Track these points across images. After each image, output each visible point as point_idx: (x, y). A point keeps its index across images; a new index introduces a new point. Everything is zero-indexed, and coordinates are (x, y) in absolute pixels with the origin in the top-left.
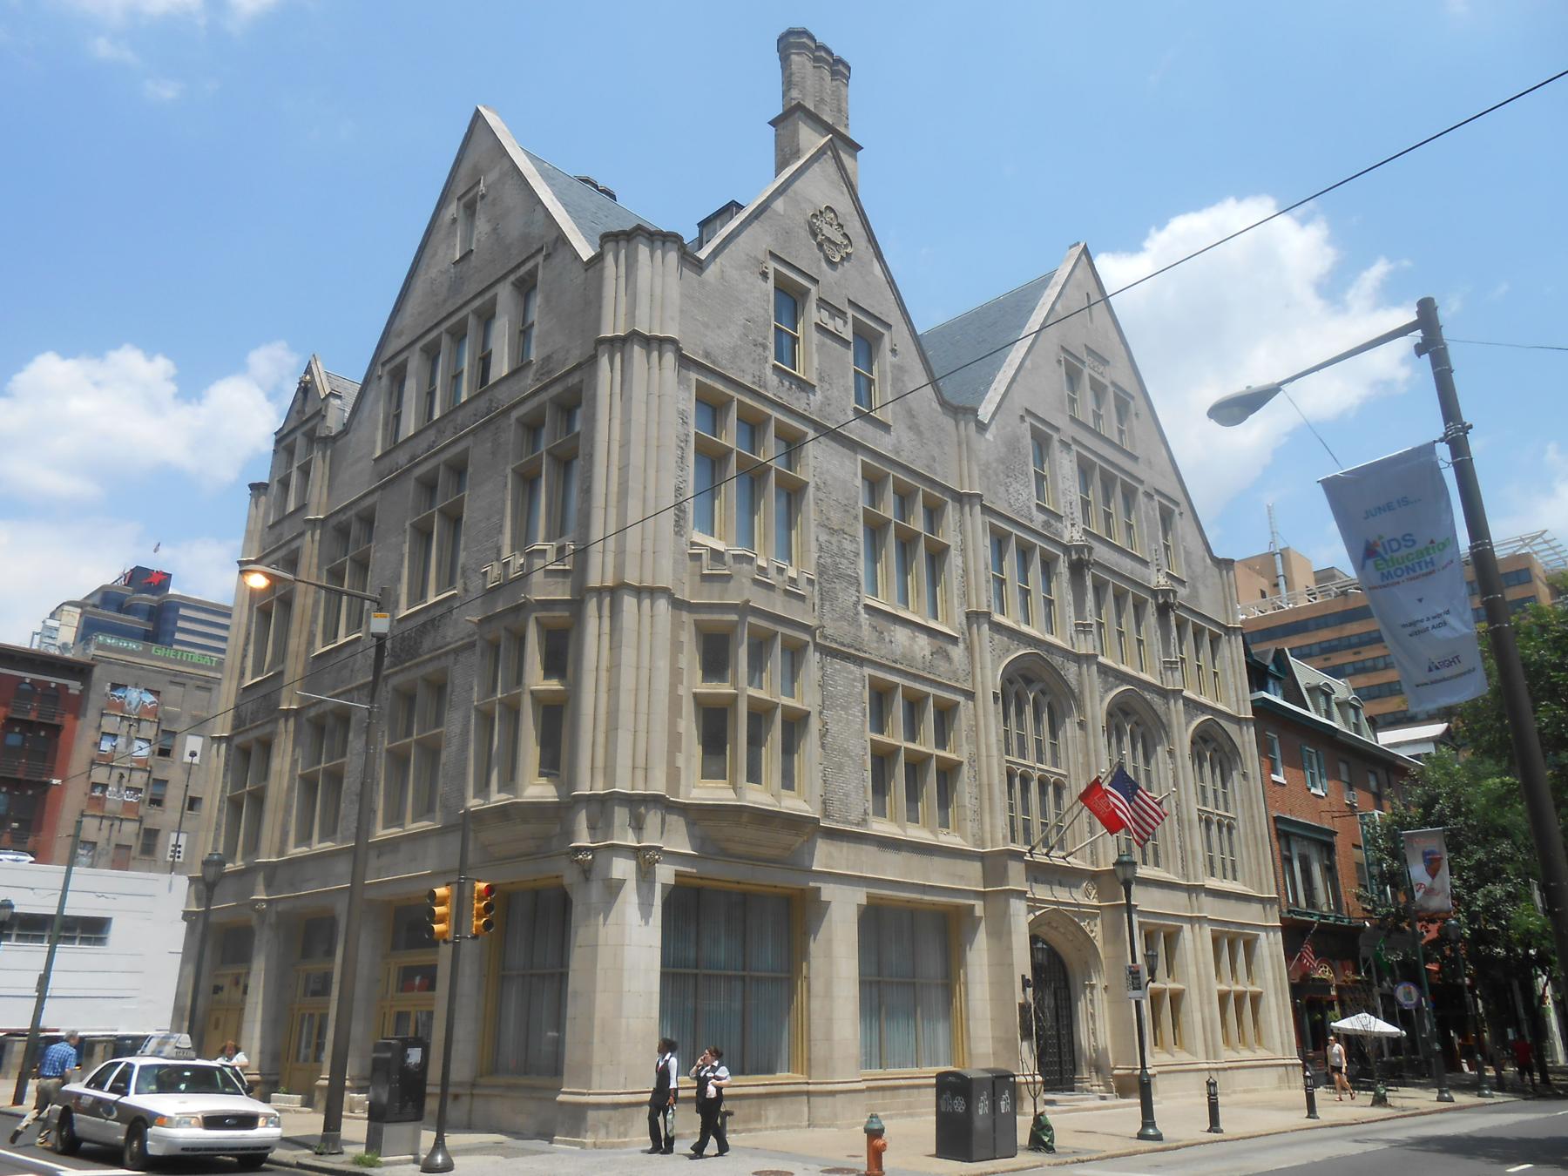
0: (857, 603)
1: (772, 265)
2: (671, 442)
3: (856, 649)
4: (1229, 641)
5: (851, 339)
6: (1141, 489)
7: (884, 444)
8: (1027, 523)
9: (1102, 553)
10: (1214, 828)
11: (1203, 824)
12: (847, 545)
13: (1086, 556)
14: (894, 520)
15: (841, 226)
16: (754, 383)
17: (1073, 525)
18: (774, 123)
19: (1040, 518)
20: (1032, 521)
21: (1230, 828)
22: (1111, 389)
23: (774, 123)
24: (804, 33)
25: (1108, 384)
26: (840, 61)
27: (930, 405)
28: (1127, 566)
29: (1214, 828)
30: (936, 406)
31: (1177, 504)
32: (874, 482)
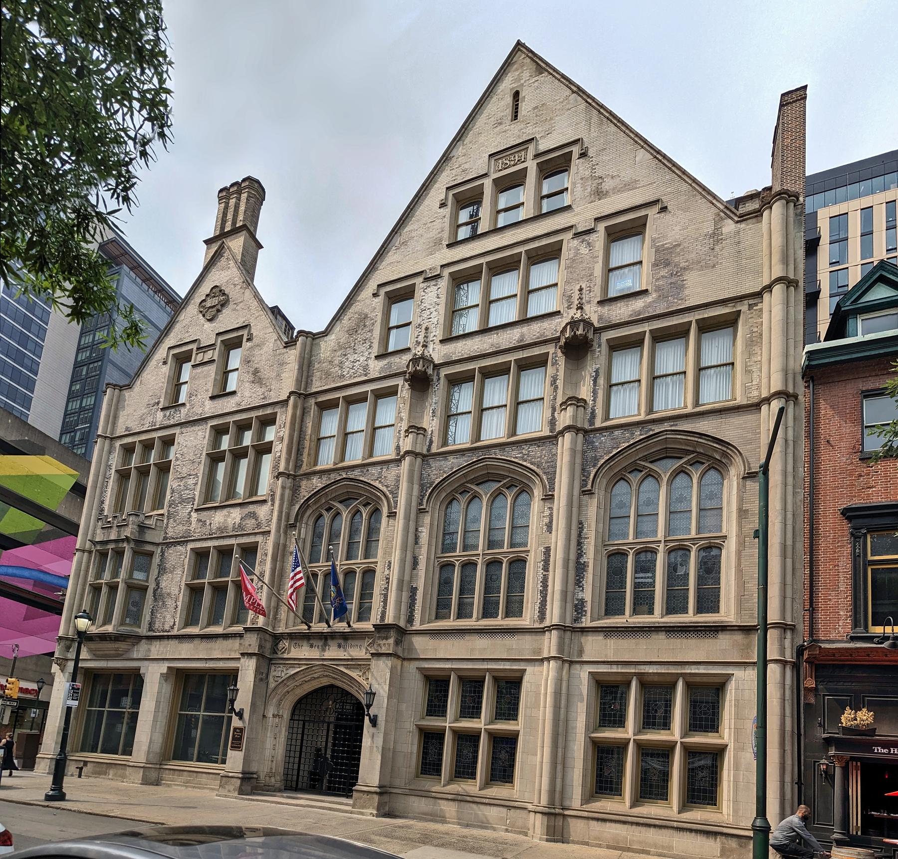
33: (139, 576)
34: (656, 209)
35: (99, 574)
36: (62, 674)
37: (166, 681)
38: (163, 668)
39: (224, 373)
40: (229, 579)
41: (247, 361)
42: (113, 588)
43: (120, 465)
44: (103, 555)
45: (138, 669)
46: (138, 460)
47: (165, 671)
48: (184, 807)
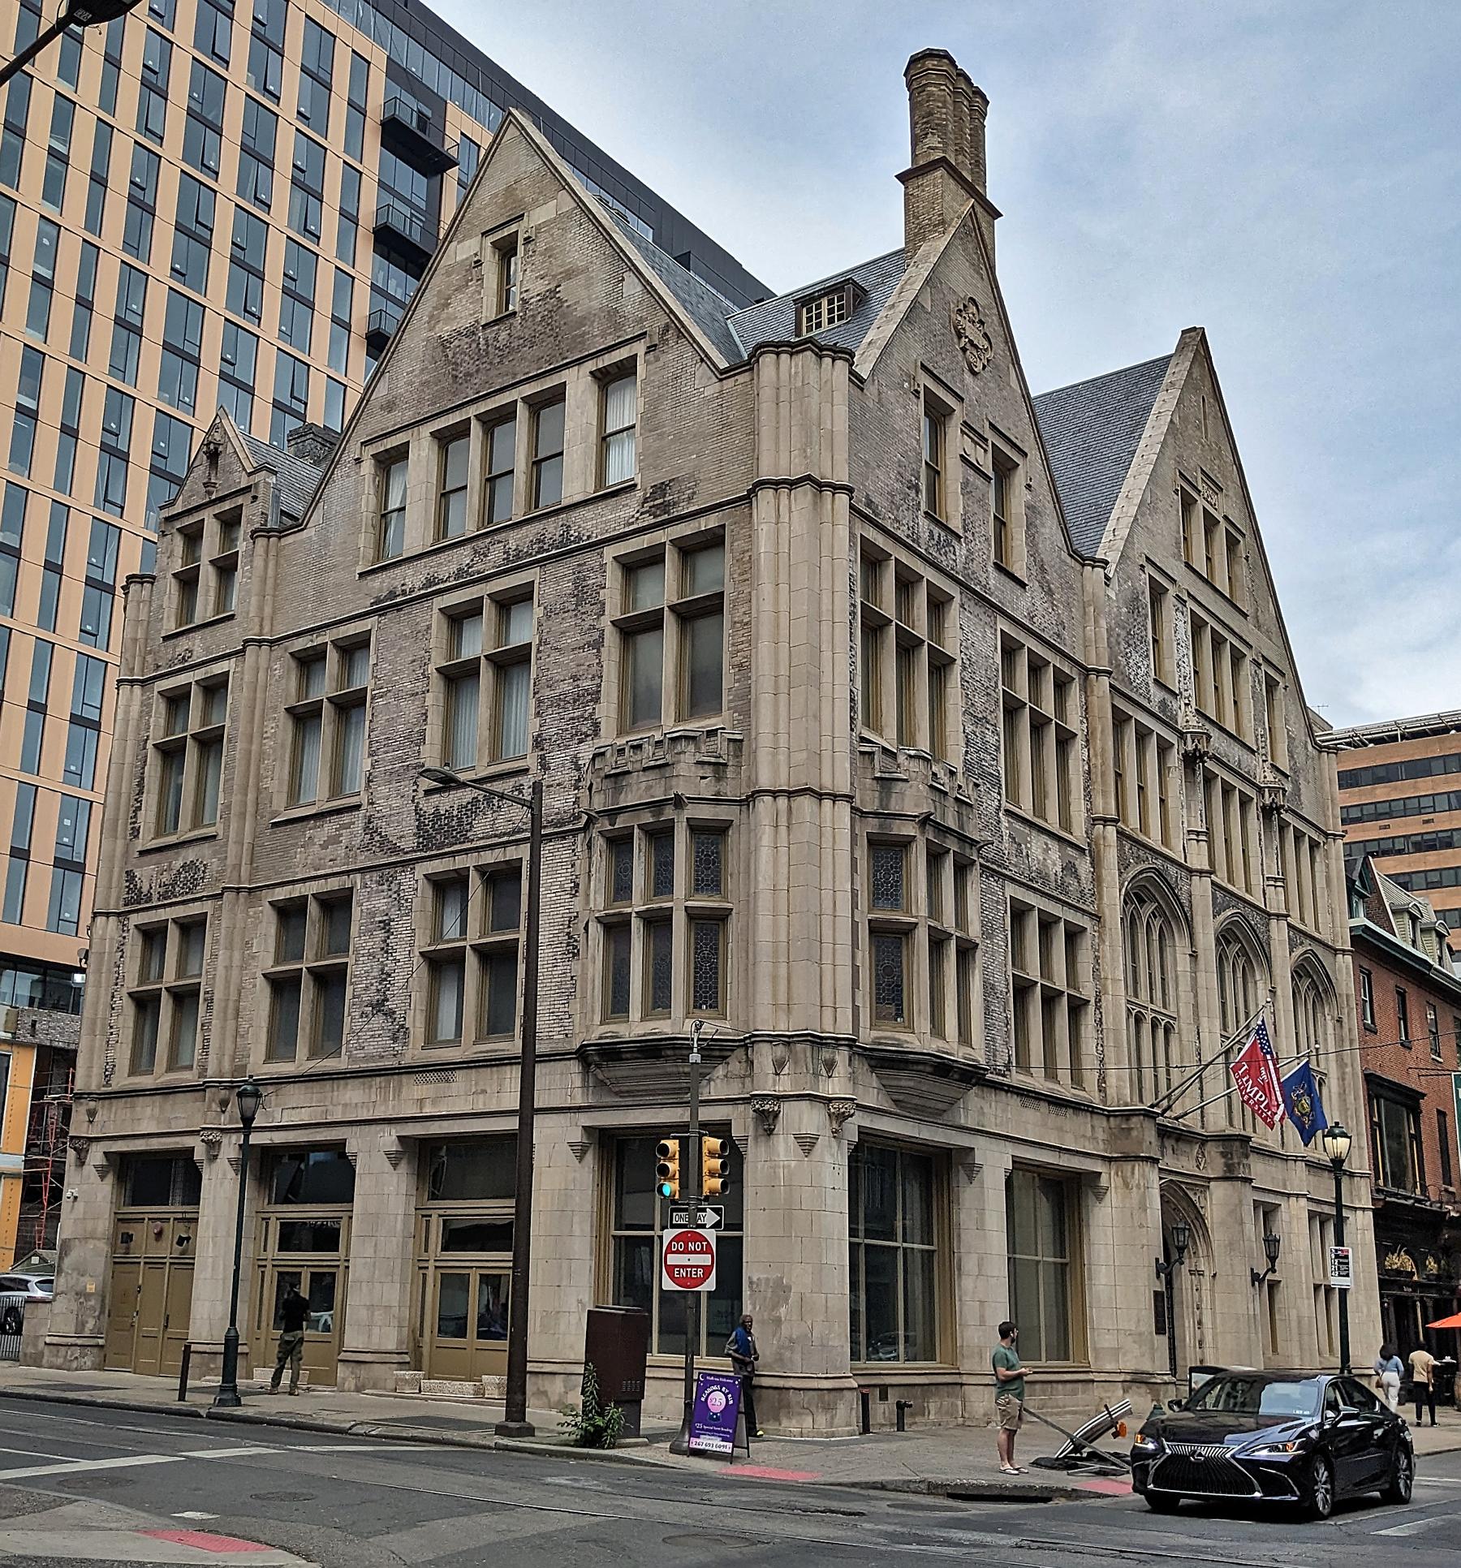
0: (998, 809)
1: (925, 380)
2: (843, 616)
3: (999, 866)
4: (789, 495)
5: (991, 474)
6: (1172, 591)
7: (1021, 604)
8: (1145, 703)
9: (1219, 744)
10: (1146, 1028)
11: (1132, 1020)
12: (991, 739)
13: (1202, 747)
14: (927, 641)
15: (982, 323)
16: (908, 536)
17: (1186, 705)
18: (903, 177)
19: (1157, 694)
20: (1150, 702)
21: (1168, 1030)
22: (1223, 524)
23: (903, 177)
24: (945, 56)
25: (1221, 519)
26: (978, 93)
27: (1059, 556)
28: (1234, 753)
29: (1146, 1028)
30: (1064, 555)
31: (1283, 675)
32: (1010, 649)
33: (1442, 803)
34: (249, 496)
35: (621, 888)
36: (834, 1142)
37: (395, 1166)
38: (388, 1138)
39: (442, 495)
40: (303, 966)
41: (650, 417)
42: (657, 923)
43: (161, 733)
44: (619, 843)
45: (342, 1143)
46: (198, 721)
47: (395, 1147)
48: (108, 1388)
